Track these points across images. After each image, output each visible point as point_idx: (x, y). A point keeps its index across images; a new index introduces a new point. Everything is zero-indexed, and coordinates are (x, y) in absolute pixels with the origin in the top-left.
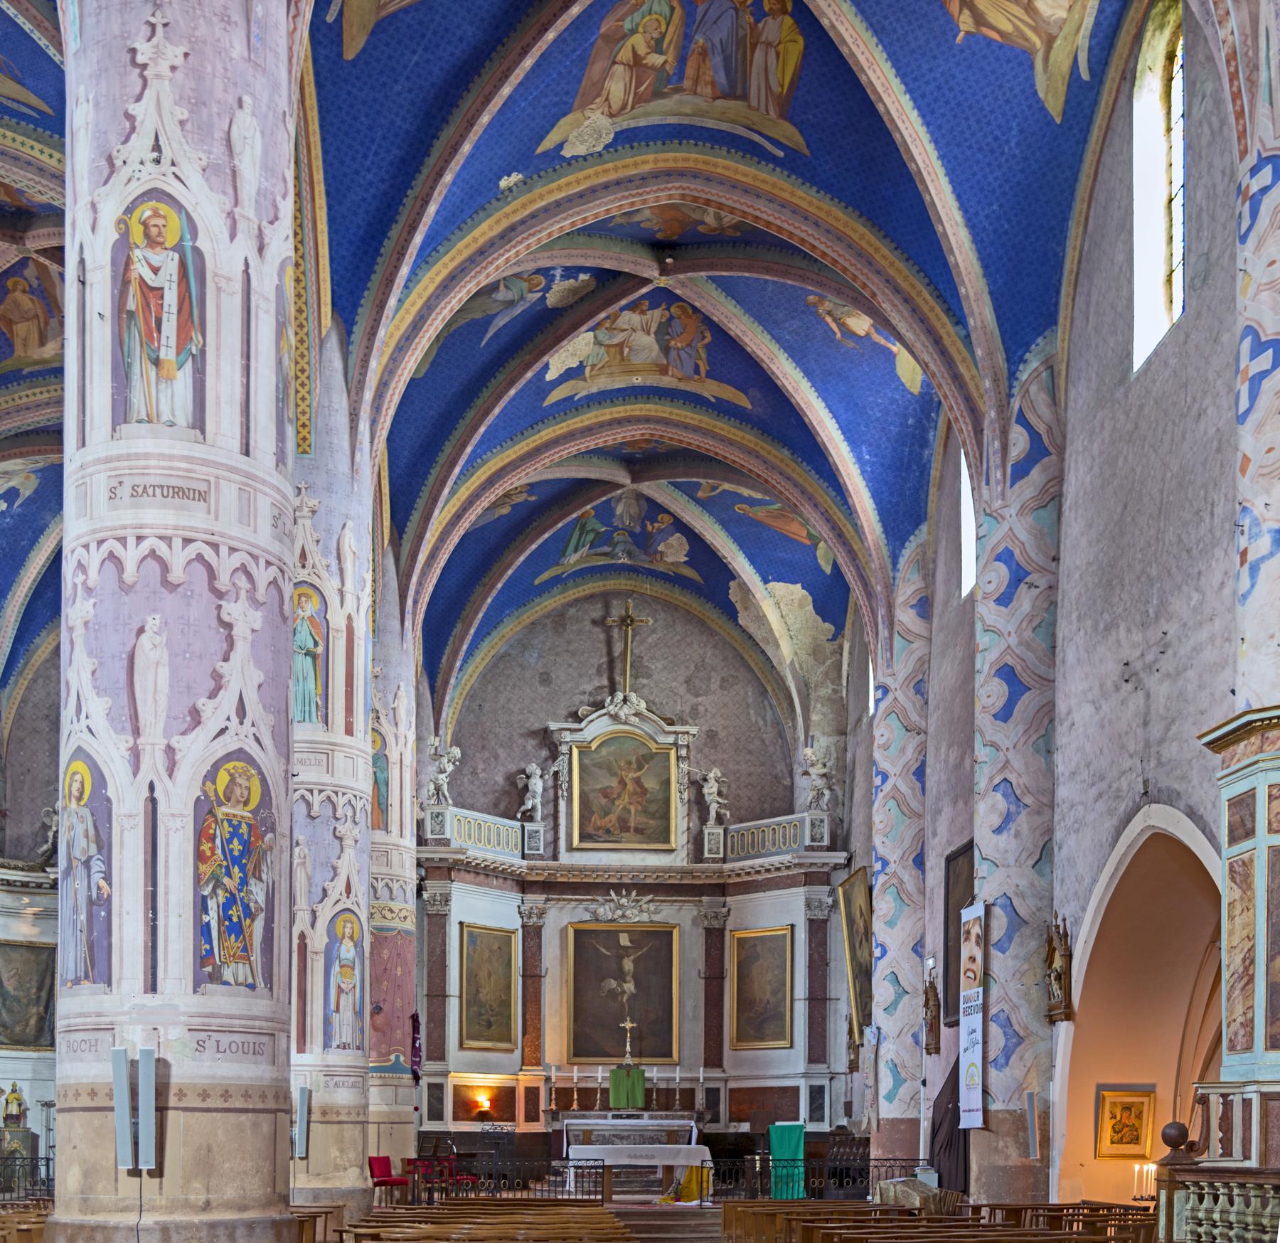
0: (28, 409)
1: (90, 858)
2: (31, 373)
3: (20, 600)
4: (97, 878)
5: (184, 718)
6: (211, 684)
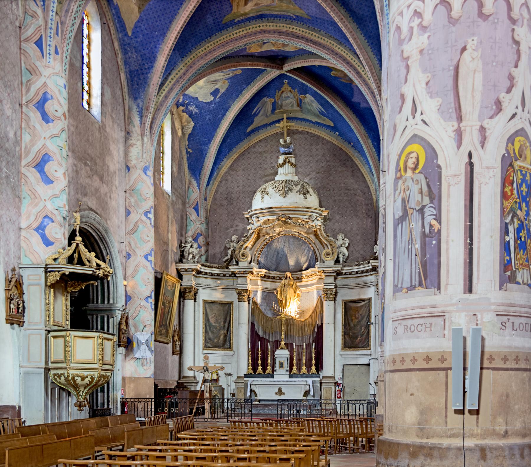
0: (236, 40)
1: (424, 207)
2: (239, 21)
3: (217, 144)
4: (429, 219)
5: (492, 107)
6: (508, 84)
